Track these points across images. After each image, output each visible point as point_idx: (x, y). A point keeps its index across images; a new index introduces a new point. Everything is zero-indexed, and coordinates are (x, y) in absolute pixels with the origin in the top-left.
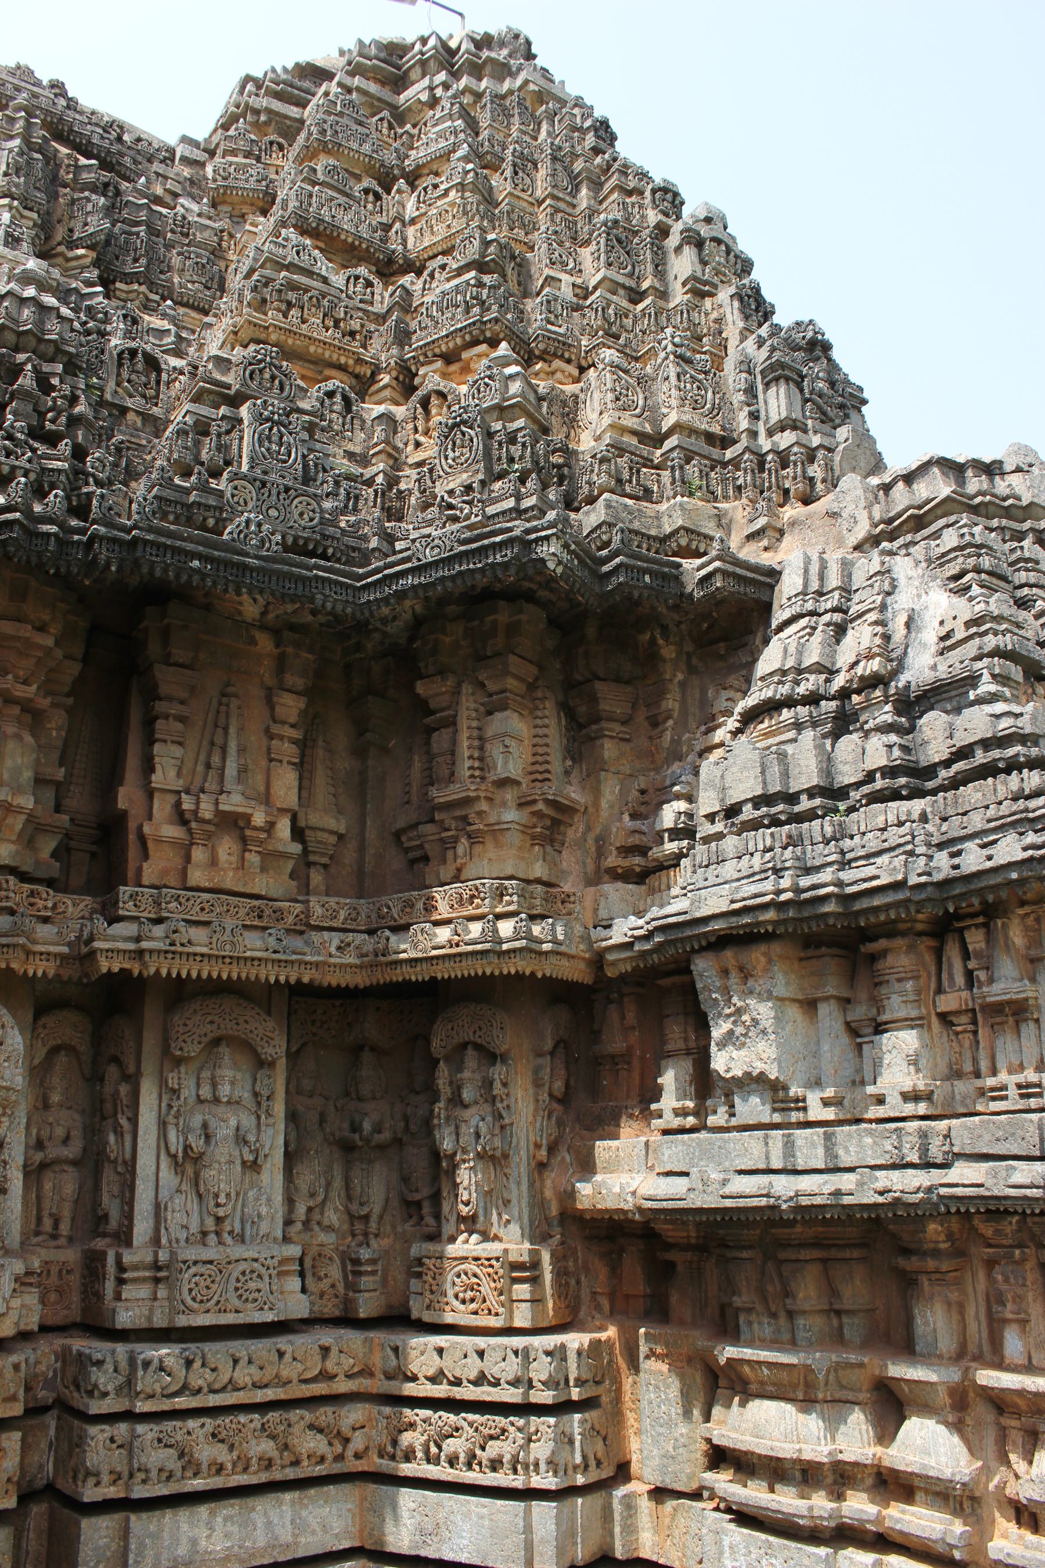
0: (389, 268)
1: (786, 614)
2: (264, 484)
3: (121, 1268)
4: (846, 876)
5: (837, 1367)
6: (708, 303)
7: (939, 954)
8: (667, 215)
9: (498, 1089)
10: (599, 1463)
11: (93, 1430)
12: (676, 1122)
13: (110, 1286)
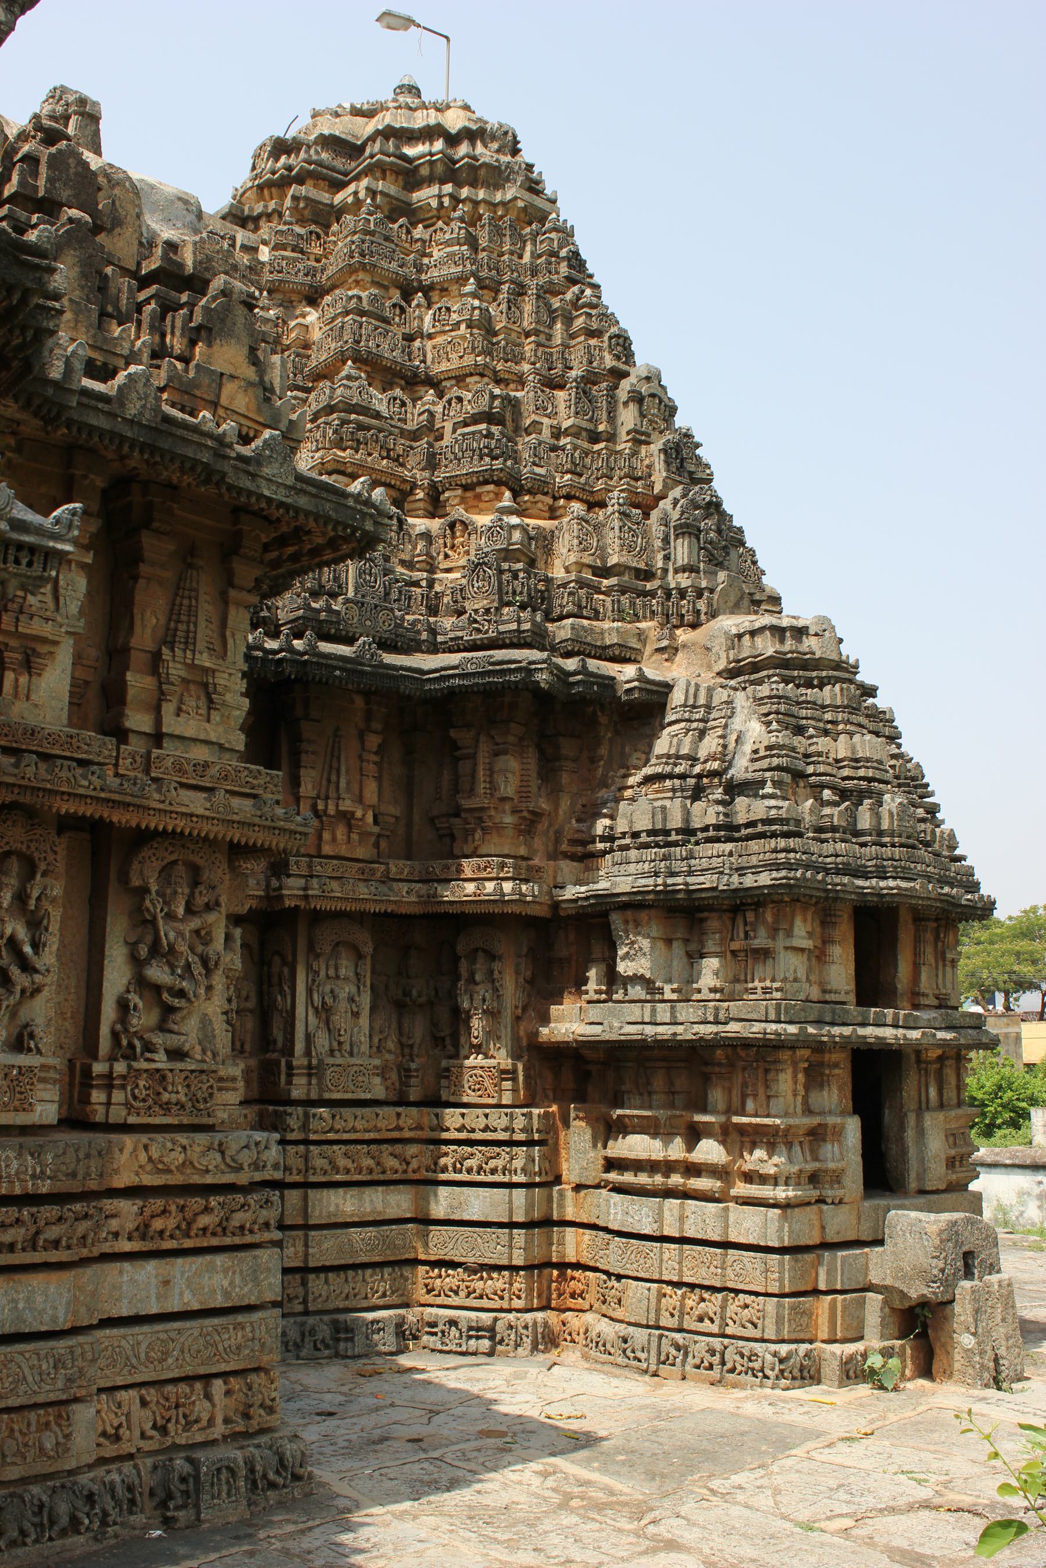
0: (414, 381)
1: (673, 718)
2: (363, 604)
4: (689, 880)
5: (671, 1117)
6: (643, 449)
9: (496, 975)
12: (596, 997)
13: (283, 1078)
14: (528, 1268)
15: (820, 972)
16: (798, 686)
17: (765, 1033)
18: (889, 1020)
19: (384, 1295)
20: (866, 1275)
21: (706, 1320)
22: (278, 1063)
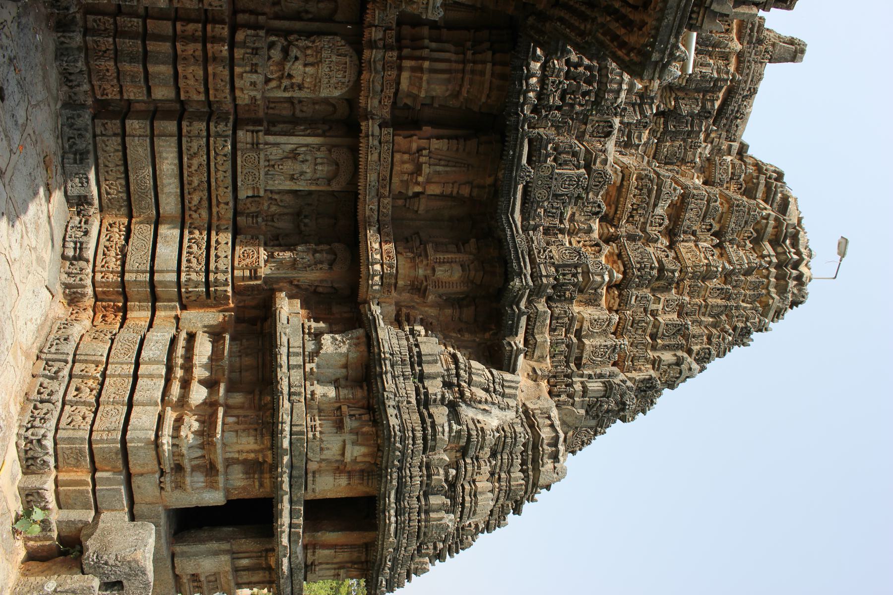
0: (672, 234)
2: (551, 178)
3: (257, 132)
4: (389, 375)
6: (650, 366)
7: (363, 408)
8: (698, 354)
9: (319, 266)
10: (187, 298)
11: (205, 124)
12: (306, 326)
13: (251, 128)
14: (123, 283)
15: (327, 470)
16: (521, 454)
17: (282, 423)
18: (295, 521)
19: (108, 193)
20: (108, 510)
21: (76, 393)
22: (261, 125)
